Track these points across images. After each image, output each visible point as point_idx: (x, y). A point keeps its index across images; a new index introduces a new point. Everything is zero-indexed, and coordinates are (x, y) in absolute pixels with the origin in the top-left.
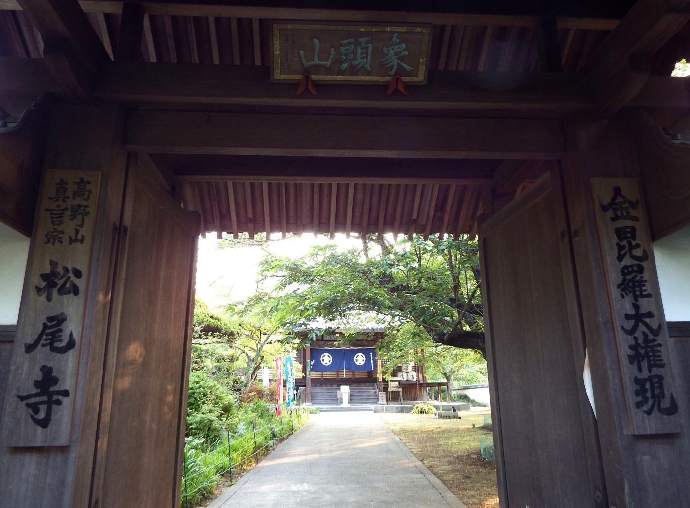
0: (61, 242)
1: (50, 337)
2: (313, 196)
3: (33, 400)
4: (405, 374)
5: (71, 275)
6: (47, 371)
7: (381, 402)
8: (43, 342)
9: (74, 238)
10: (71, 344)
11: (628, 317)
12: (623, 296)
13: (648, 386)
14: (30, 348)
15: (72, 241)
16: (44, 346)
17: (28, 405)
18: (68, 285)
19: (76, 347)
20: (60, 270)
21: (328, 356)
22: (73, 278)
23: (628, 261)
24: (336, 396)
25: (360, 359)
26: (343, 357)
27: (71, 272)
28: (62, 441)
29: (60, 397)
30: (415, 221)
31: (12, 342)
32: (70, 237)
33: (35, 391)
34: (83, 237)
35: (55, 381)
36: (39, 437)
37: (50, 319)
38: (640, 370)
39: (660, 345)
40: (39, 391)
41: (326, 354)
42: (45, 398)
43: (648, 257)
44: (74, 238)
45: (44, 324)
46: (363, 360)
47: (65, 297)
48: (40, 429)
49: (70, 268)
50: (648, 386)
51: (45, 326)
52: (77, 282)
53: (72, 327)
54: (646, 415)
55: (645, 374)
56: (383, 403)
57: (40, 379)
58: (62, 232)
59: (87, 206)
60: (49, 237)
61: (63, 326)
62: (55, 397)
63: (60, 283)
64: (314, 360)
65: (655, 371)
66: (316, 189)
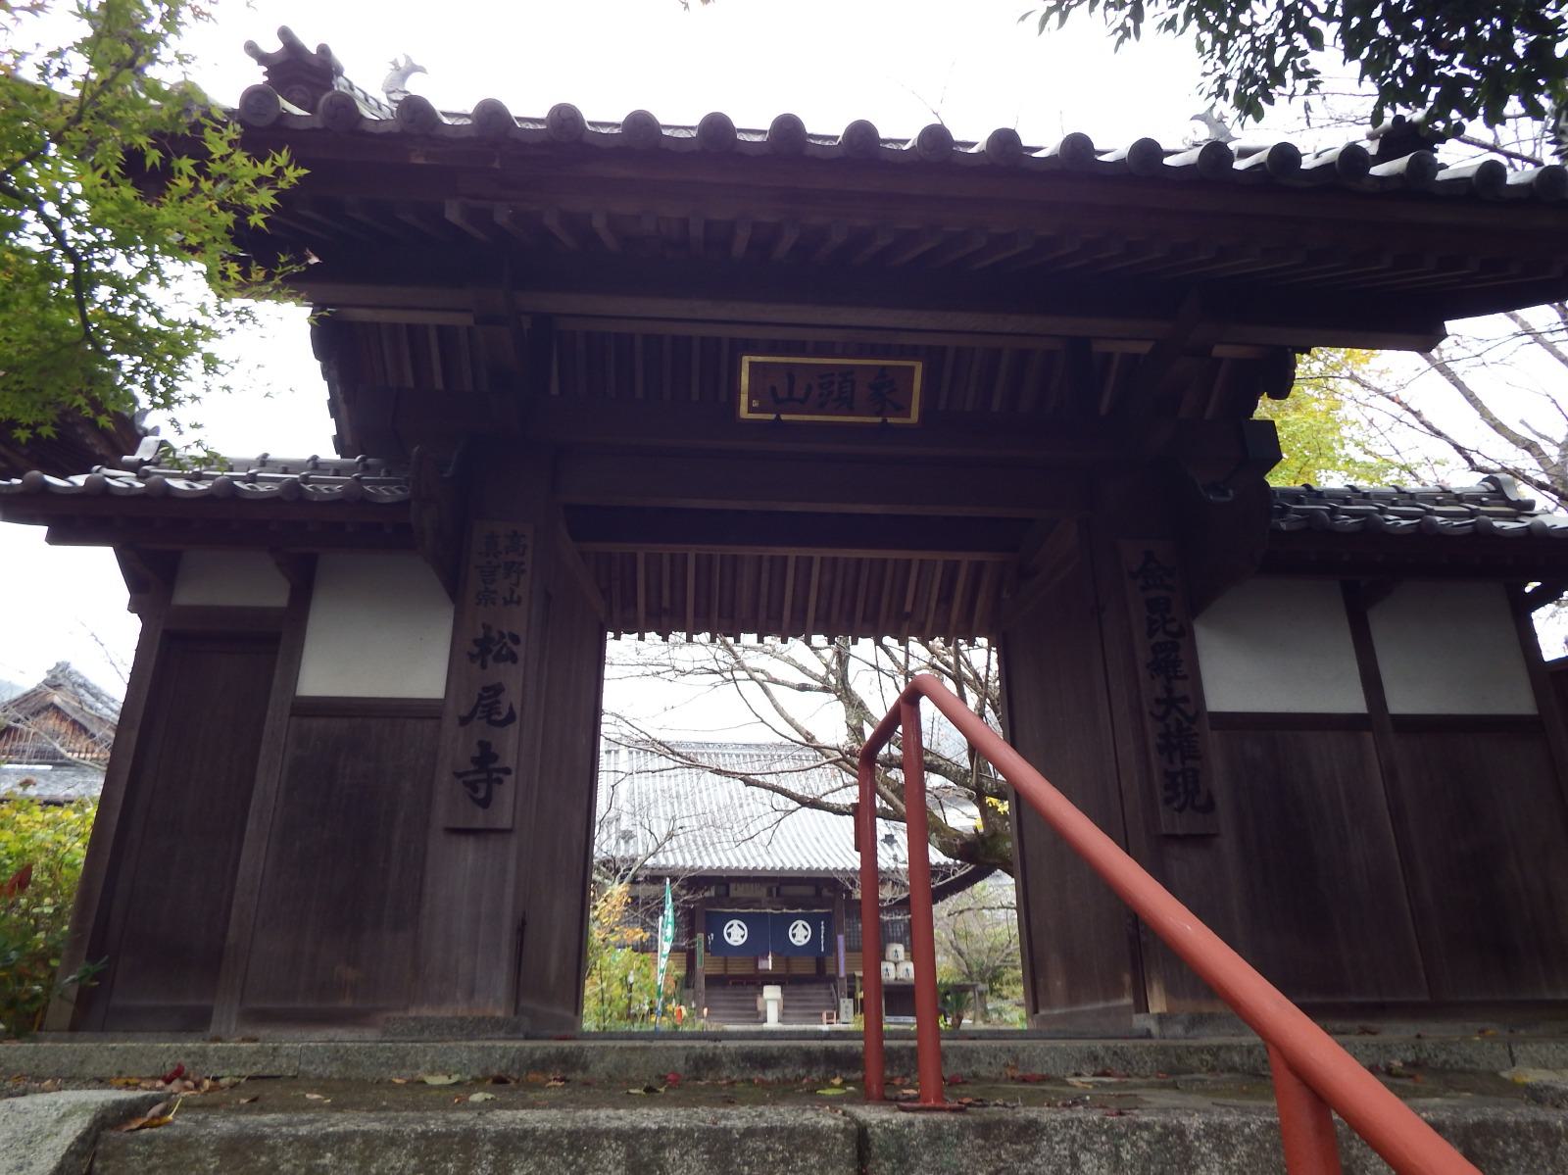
0: (494, 603)
1: (486, 709)
2: (760, 573)
3: (471, 778)
4: (891, 966)
5: (507, 640)
6: (484, 746)
7: (843, 1018)
8: (479, 714)
9: (508, 599)
10: (511, 717)
11: (1158, 701)
12: (1153, 677)
13: (1180, 780)
14: (464, 721)
15: (506, 602)
16: (480, 718)
17: (464, 783)
18: (504, 652)
19: (518, 722)
20: (495, 634)
21: (739, 925)
22: (510, 644)
23: (1160, 637)
24: (756, 1008)
25: (800, 934)
26: (768, 932)
27: (507, 637)
28: (505, 822)
29: (501, 775)
30: (908, 616)
31: (439, 718)
32: (504, 598)
33: (472, 768)
34: (519, 598)
35: (495, 758)
36: (480, 819)
37: (486, 689)
38: (1171, 762)
39: (1196, 734)
40: (477, 768)
41: (735, 922)
42: (483, 776)
43: (1187, 633)
44: (508, 599)
45: (480, 695)
46: (806, 937)
47: (501, 666)
48: (480, 811)
49: (505, 632)
50: (1180, 780)
51: (481, 698)
52: (514, 648)
53: (512, 697)
54: (1176, 813)
55: (1178, 766)
56: (846, 1021)
57: (477, 755)
58: (495, 592)
59: (522, 563)
60: (481, 597)
61: (502, 697)
62: (495, 775)
63: (495, 649)
64: (712, 935)
65: (1190, 763)
66: (766, 565)
